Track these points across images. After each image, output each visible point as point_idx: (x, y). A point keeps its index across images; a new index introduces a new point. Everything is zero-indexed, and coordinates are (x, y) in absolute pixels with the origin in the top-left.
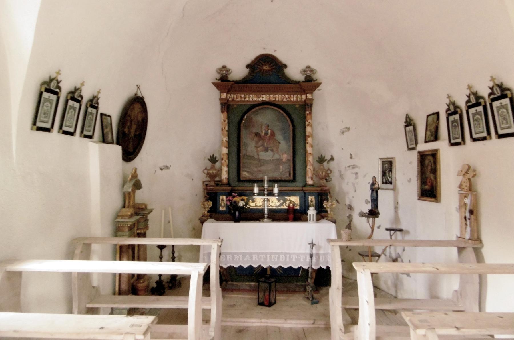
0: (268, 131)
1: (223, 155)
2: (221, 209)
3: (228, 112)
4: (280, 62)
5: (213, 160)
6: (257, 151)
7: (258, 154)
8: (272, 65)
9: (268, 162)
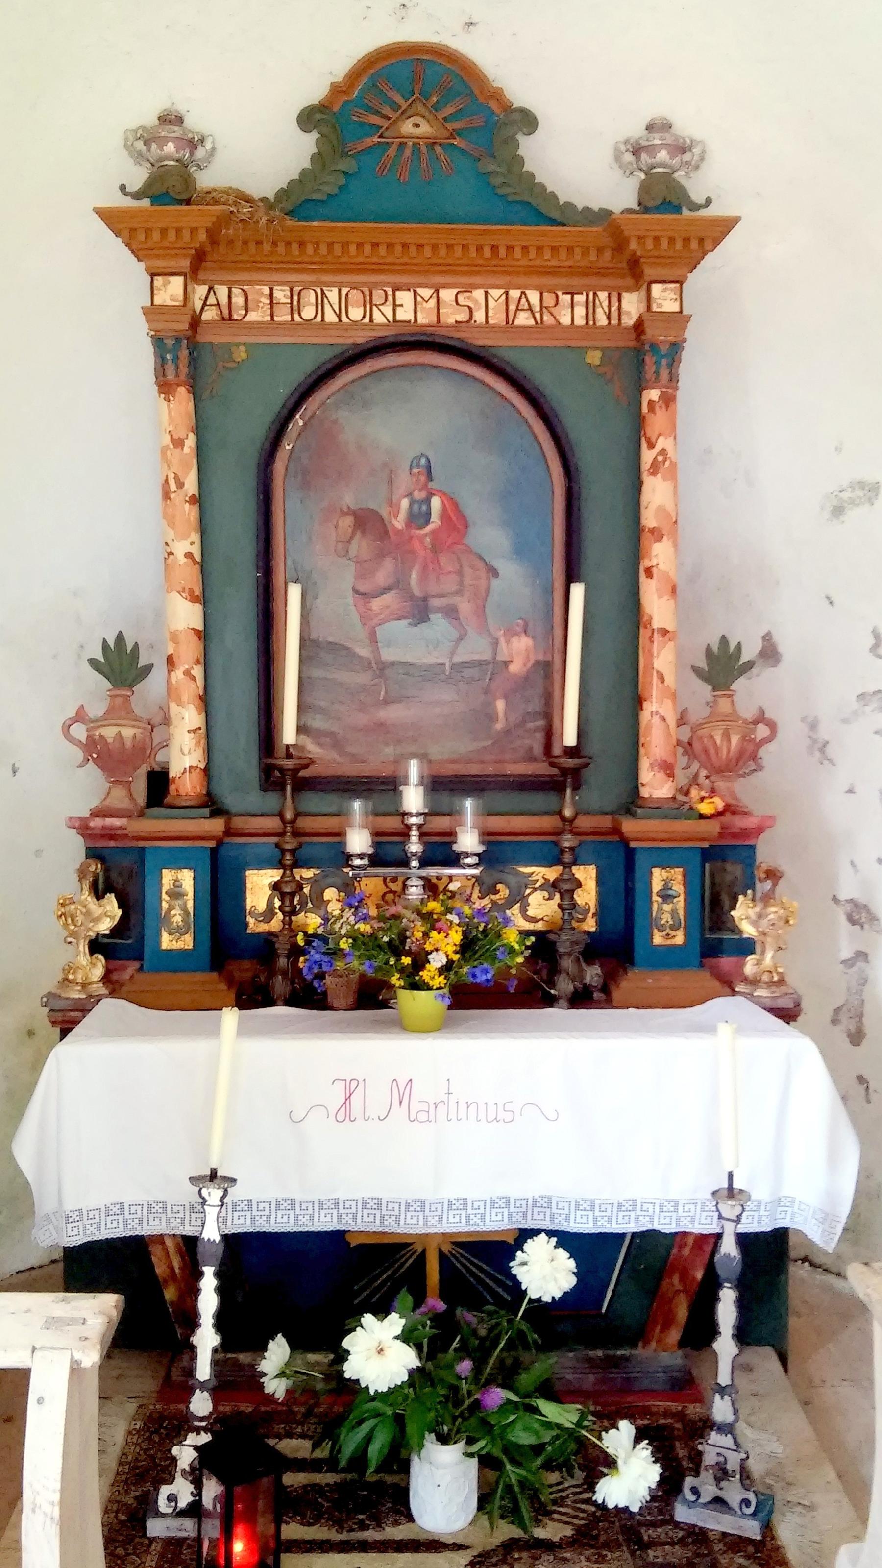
0: (428, 501)
1: (174, 637)
2: (167, 942)
4: (497, 95)
5: (121, 665)
6: (365, 619)
7: (373, 638)
8: (449, 110)
9: (431, 674)
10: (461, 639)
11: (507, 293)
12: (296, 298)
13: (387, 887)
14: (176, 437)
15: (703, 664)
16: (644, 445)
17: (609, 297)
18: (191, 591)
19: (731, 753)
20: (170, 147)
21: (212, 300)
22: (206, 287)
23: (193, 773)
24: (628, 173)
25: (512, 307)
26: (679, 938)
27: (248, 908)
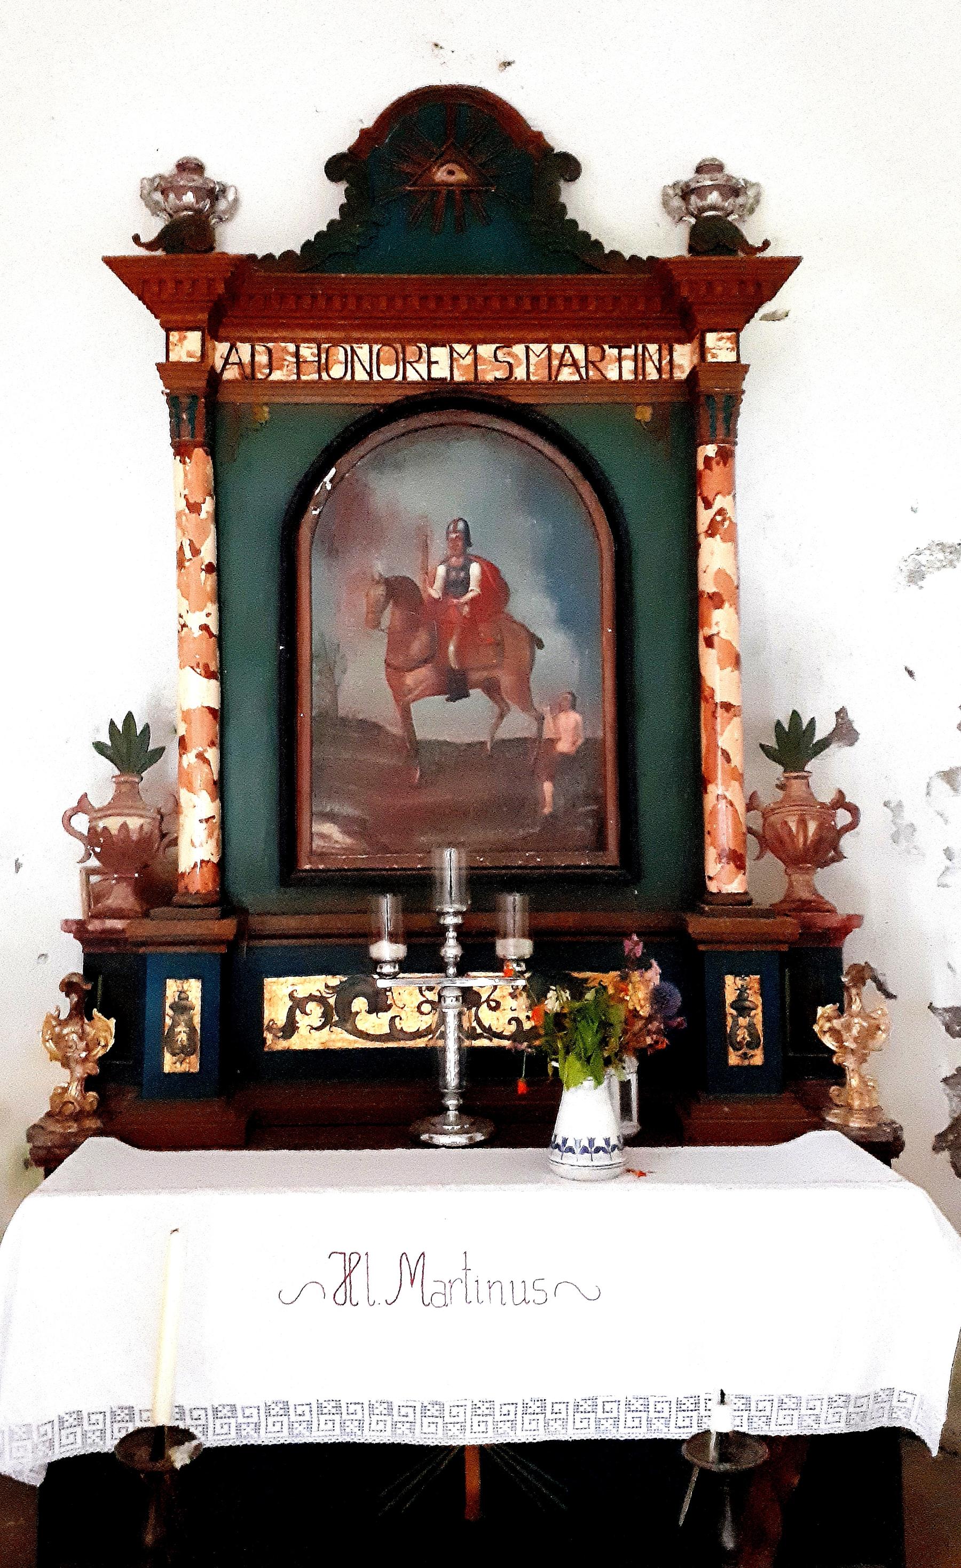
0: (466, 568)
1: (187, 716)
2: (170, 1064)
3: (212, 452)
5: (129, 748)
10: (501, 716)
11: (549, 348)
12: (323, 356)
13: (424, 996)
14: (192, 501)
15: (772, 742)
16: (700, 504)
17: (660, 350)
18: (206, 666)
19: (809, 842)
20: (189, 198)
21: (234, 358)
22: (228, 345)
23: (205, 869)
24: (677, 218)
25: (555, 363)
26: (758, 1059)
27: (266, 1022)
